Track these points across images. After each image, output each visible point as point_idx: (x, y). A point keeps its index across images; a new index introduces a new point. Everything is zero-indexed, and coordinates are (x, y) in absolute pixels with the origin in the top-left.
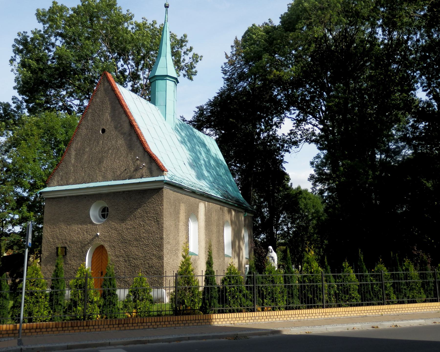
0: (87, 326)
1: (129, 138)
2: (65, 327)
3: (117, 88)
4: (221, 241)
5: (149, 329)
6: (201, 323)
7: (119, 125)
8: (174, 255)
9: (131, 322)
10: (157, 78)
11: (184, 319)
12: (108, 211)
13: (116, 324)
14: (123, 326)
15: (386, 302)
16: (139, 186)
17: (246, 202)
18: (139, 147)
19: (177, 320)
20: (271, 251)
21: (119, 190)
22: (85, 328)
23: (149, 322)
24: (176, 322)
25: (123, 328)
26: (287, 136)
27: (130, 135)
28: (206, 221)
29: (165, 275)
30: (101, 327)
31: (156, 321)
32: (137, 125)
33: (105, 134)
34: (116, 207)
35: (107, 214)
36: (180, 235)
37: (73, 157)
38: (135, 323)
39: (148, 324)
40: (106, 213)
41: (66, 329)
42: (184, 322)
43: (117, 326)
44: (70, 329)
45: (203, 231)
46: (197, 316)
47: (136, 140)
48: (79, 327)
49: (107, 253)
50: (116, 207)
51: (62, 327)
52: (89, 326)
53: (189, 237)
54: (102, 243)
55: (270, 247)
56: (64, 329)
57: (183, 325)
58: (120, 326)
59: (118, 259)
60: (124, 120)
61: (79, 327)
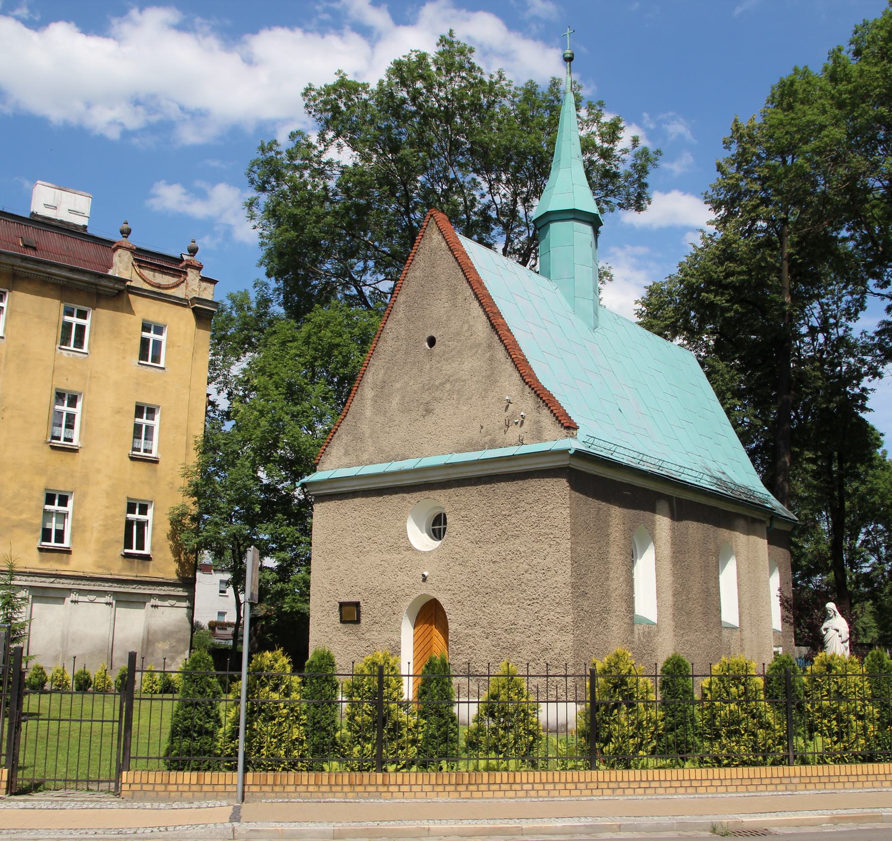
0: (384, 784)
1: (488, 354)
2: (336, 785)
3: (459, 243)
4: (713, 590)
5: (529, 800)
6: (717, 786)
7: (466, 327)
8: (599, 624)
9: (466, 781)
10: (552, 218)
11: (613, 779)
12: (445, 523)
13: (450, 784)
14: (467, 791)
15: (193, 764)
16: (513, 463)
17: (772, 497)
18: (511, 375)
19: (594, 779)
20: (832, 614)
21: (470, 474)
22: (381, 789)
23: (528, 783)
24: (594, 785)
25: (468, 794)
26: (873, 338)
27: (490, 346)
28: (673, 544)
29: (658, 678)
30: (415, 788)
31: (544, 780)
32: (505, 325)
33: (437, 348)
34: (463, 513)
35: (445, 529)
36: (611, 576)
37: (369, 403)
38: (495, 783)
39: (526, 787)
40: (442, 527)
41: (339, 788)
42: (612, 785)
43: (453, 788)
44: (346, 789)
45: (667, 566)
46: (550, 774)
47: (503, 359)
48: (365, 786)
49: (446, 617)
50: (463, 513)
51: (329, 784)
52: (390, 785)
53: (632, 580)
54: (435, 595)
55: (831, 606)
56: (334, 789)
57: (609, 792)
58: (460, 788)
59: (470, 632)
60: (475, 314)
61: (365, 786)
